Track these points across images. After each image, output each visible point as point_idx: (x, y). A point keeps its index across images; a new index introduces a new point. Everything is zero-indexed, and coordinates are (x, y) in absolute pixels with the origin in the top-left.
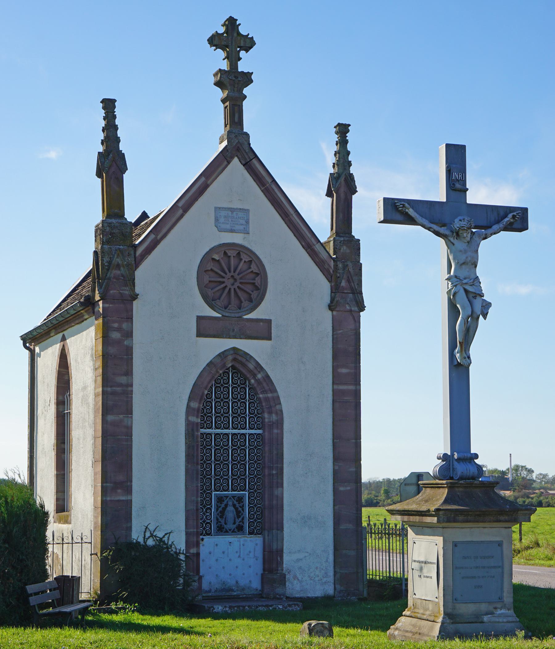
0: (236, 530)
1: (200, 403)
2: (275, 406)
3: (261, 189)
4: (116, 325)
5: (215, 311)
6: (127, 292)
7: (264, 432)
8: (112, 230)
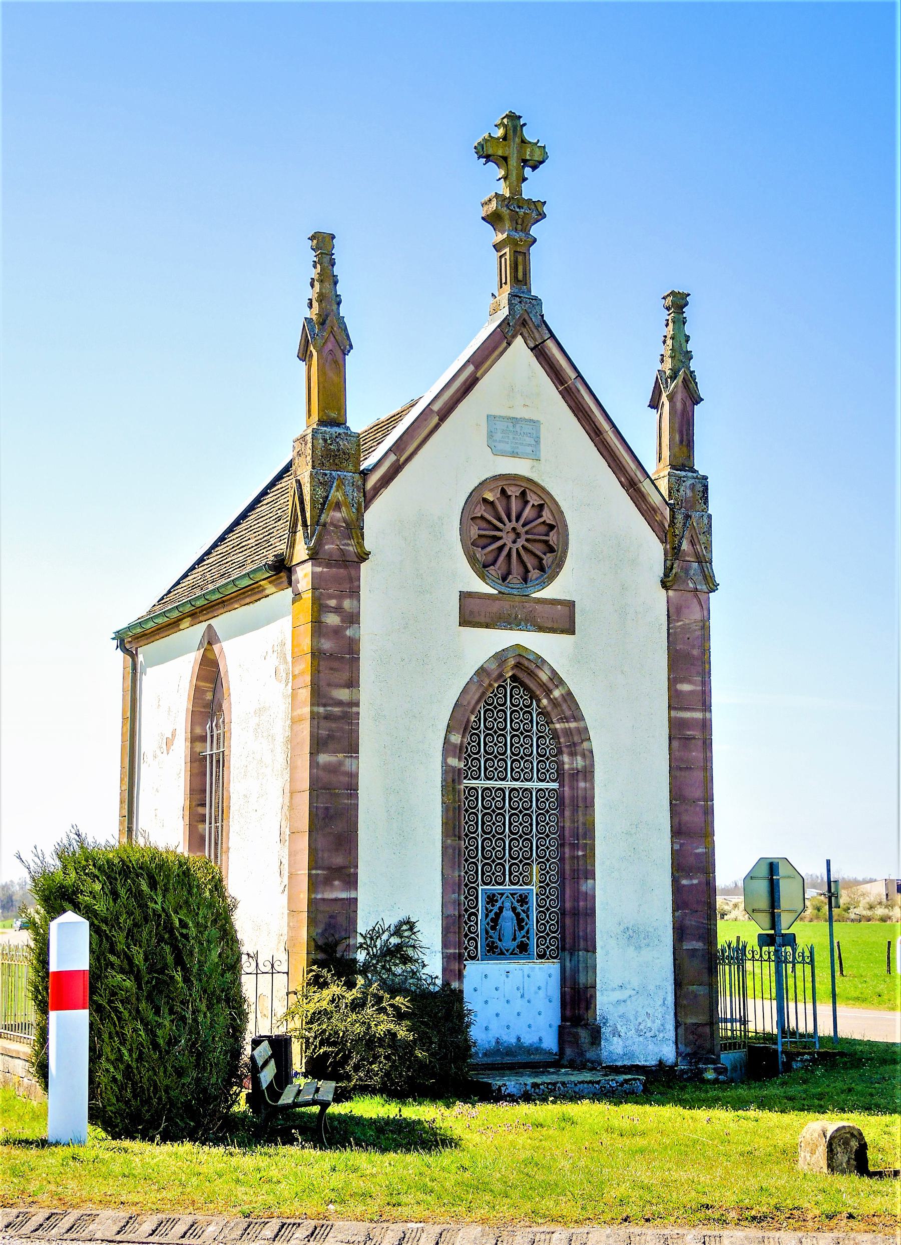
0: (517, 951)
1: (463, 737)
2: (582, 742)
4: (333, 603)
6: (351, 548)
7: (562, 785)
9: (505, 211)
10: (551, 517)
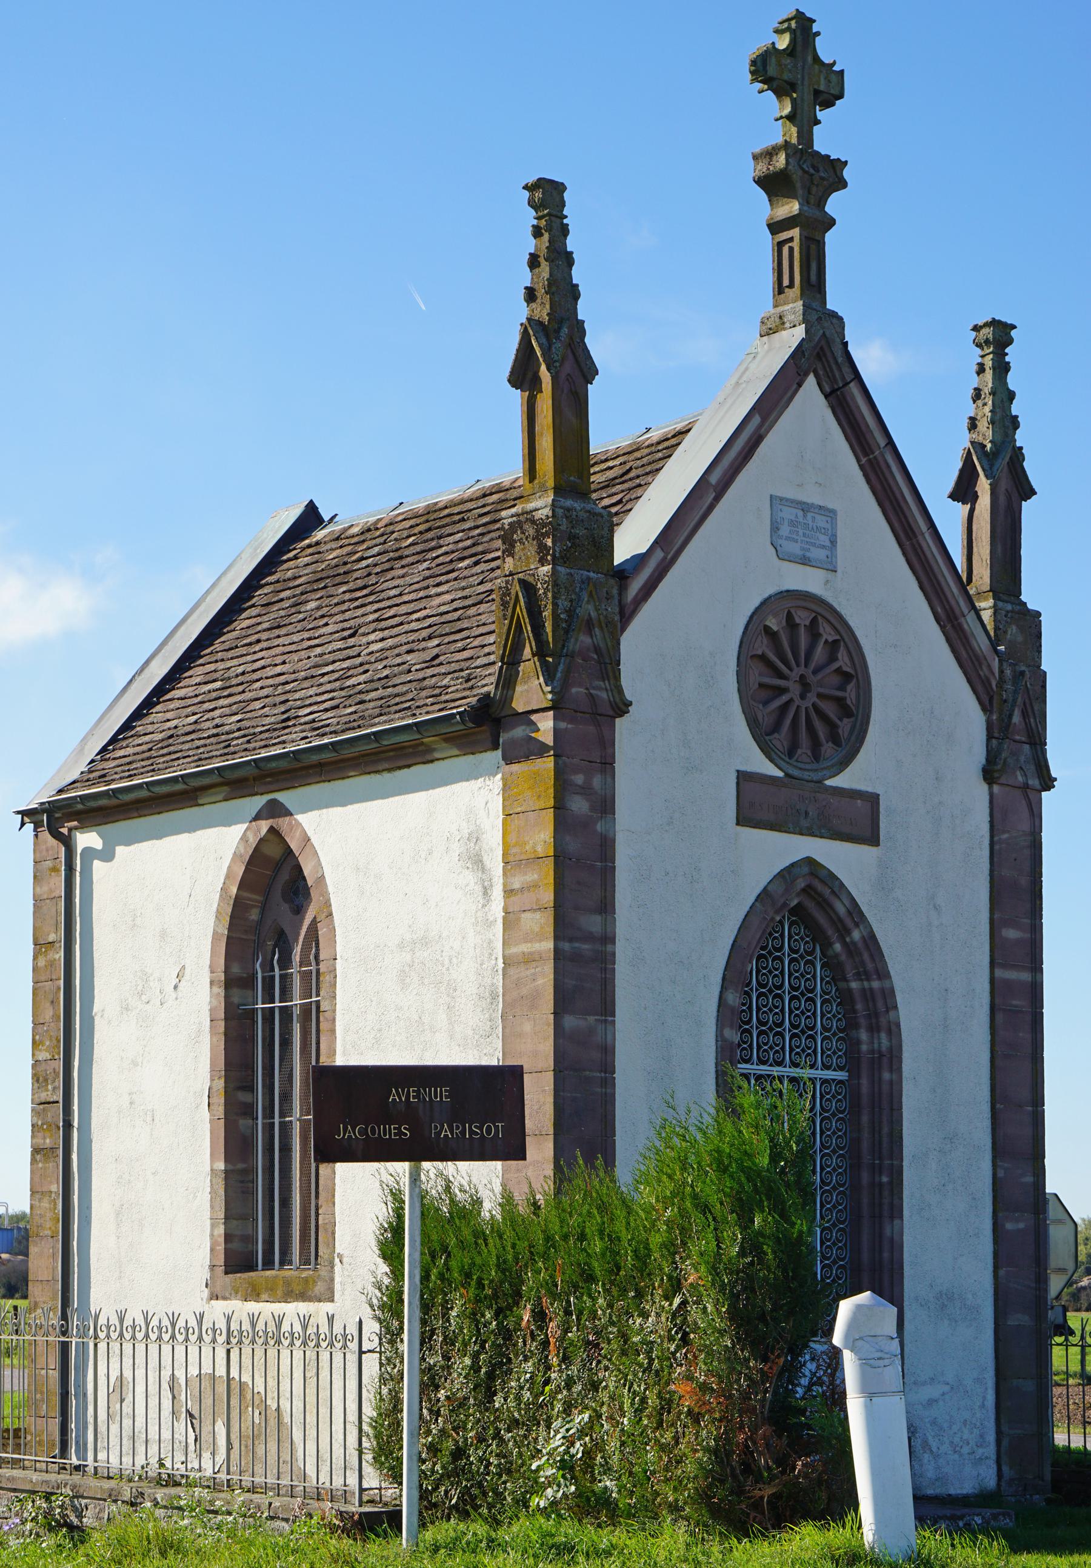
3: (858, 460)
4: (579, 779)
5: (772, 760)
6: (604, 695)
8: (573, 527)
9: (796, 176)
10: (848, 662)
